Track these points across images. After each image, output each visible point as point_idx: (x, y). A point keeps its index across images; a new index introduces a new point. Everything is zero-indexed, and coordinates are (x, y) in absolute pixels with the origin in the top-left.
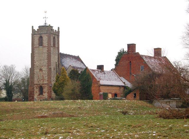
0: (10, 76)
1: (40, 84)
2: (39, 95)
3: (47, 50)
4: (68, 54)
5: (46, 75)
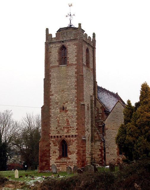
0: (3, 129)
1: (61, 137)
2: (60, 157)
3: (76, 70)
4: (103, 87)
5: (74, 119)
